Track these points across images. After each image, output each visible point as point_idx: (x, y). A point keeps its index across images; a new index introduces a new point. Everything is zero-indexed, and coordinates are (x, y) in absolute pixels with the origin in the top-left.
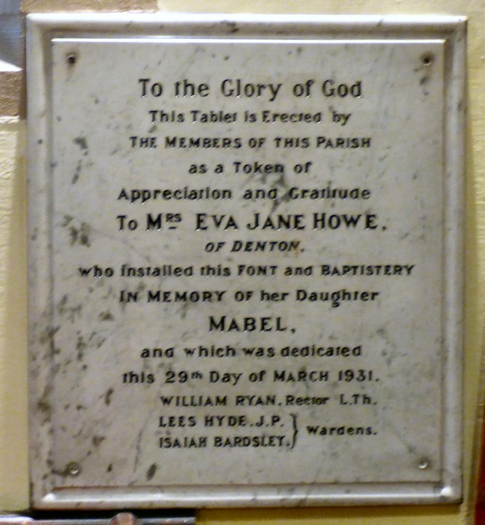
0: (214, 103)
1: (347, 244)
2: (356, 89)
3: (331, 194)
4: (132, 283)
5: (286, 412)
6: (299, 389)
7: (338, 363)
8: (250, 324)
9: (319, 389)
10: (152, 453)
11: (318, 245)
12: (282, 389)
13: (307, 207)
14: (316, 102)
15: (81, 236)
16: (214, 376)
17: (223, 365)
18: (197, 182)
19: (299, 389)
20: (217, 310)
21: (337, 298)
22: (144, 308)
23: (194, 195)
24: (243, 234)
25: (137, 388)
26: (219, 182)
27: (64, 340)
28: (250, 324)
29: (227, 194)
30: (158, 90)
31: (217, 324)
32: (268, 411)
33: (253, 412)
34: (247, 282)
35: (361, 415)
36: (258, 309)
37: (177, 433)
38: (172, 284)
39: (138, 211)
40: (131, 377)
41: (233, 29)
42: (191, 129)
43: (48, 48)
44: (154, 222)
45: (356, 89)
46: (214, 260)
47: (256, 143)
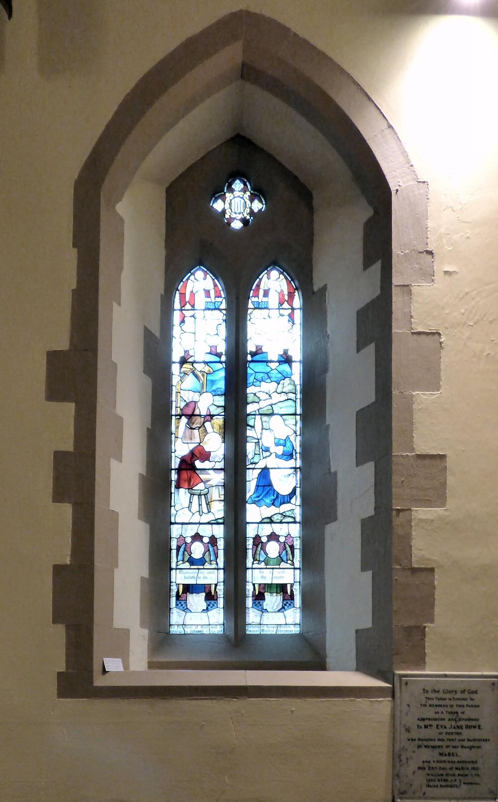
0: (441, 695)
1: (475, 733)
2: (476, 692)
3: (470, 720)
4: (420, 743)
5: (458, 778)
6: (461, 772)
7: (470, 766)
8: (449, 754)
9: (467, 772)
10: (424, 789)
11: (466, 733)
12: (457, 772)
13: (463, 723)
14: (466, 695)
15: (408, 730)
16: (440, 768)
17: (442, 765)
18: (437, 716)
19: (461, 772)
20: (441, 751)
21: (471, 748)
22: (424, 750)
23: (435, 720)
24: (448, 730)
25: (420, 771)
26: (442, 716)
27: (403, 758)
28: (449, 754)
29: (444, 719)
30: (427, 692)
31: (441, 754)
32: (453, 778)
33: (450, 778)
34: (449, 743)
35: (477, 779)
36: (452, 750)
37: (431, 783)
38: (432, 743)
39: (422, 724)
40: (420, 768)
41: (446, 676)
42: (436, 702)
43: (401, 680)
44: (426, 727)
45: (476, 692)
46: (441, 737)
47: (452, 706)
